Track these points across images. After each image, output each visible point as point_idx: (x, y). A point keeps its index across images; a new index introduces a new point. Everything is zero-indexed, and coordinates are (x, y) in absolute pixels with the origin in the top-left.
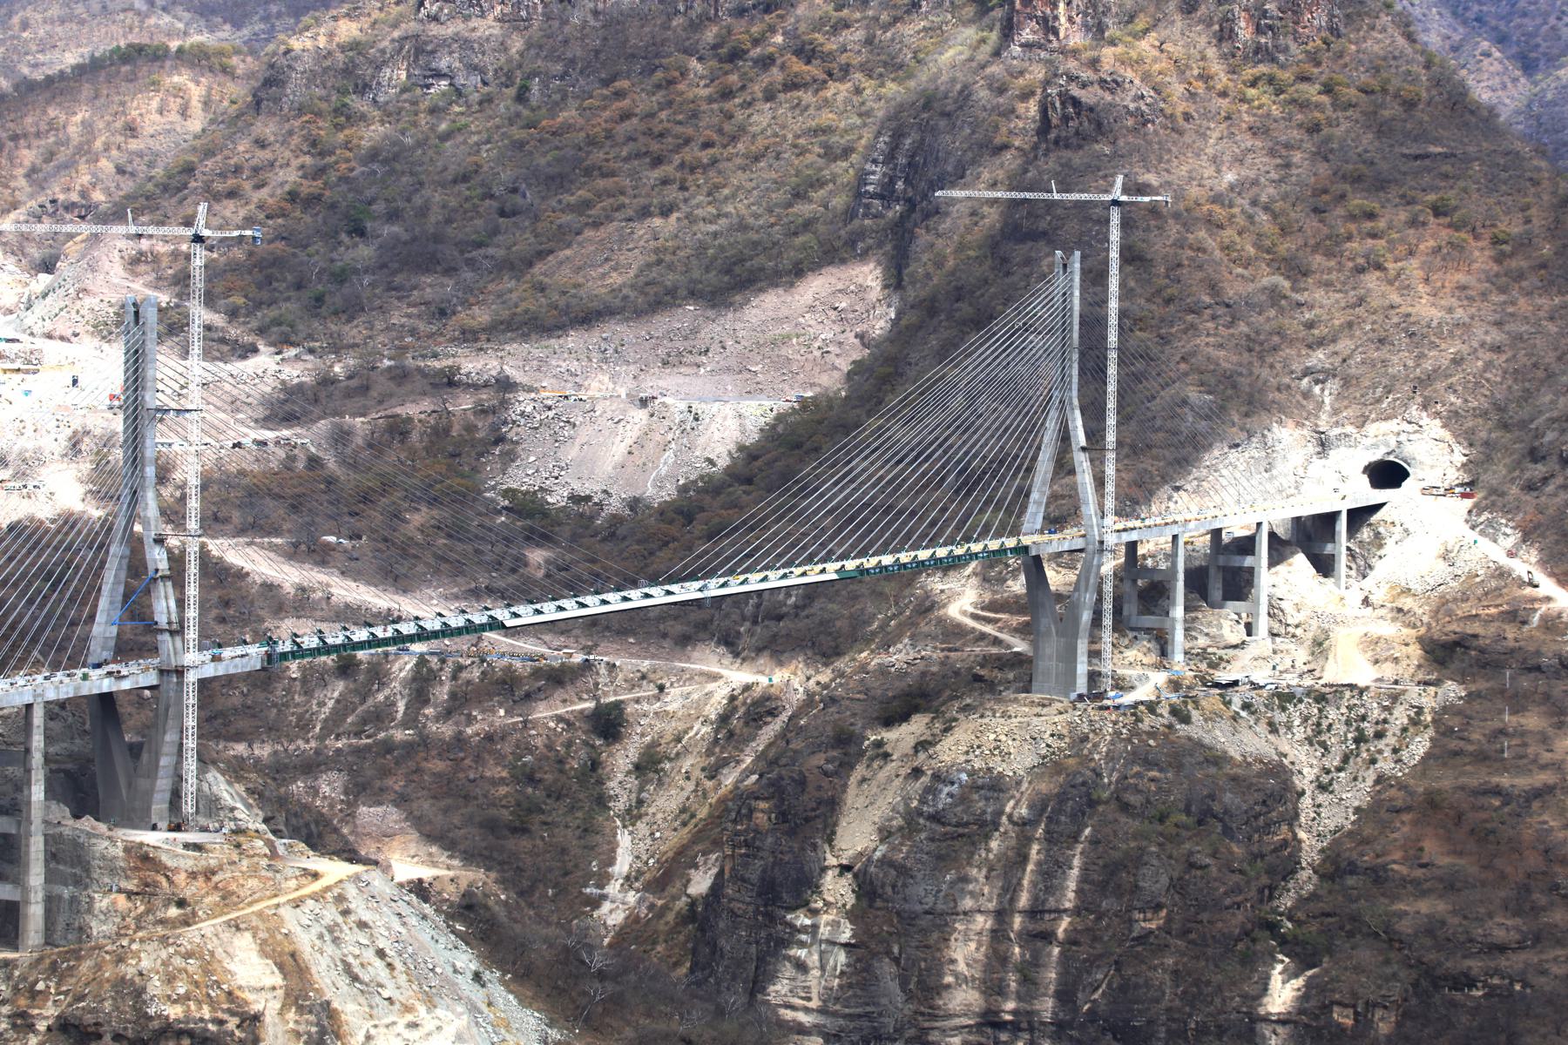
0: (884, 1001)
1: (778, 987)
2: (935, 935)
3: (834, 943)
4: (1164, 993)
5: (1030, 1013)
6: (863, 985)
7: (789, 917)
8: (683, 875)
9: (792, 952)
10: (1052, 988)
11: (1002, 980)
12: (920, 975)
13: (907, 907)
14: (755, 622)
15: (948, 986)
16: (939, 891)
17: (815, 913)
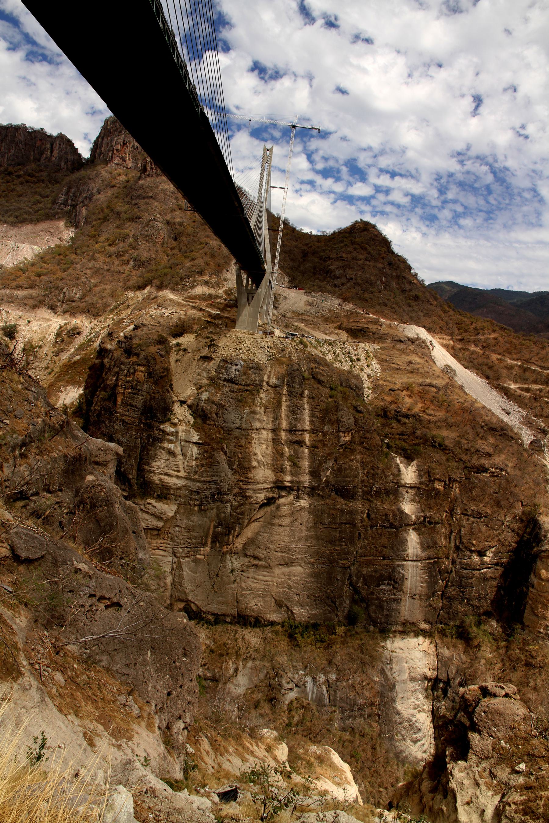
0: (223, 474)
1: (158, 463)
2: (243, 440)
3: (189, 442)
4: (358, 473)
5: (298, 482)
6: (210, 465)
7: (162, 427)
8: (56, 395)
9: (166, 445)
10: (307, 471)
11: (282, 465)
12: (239, 461)
13: (226, 425)
14: (63, 302)
15: (255, 467)
16: (242, 418)
17: (174, 425)
